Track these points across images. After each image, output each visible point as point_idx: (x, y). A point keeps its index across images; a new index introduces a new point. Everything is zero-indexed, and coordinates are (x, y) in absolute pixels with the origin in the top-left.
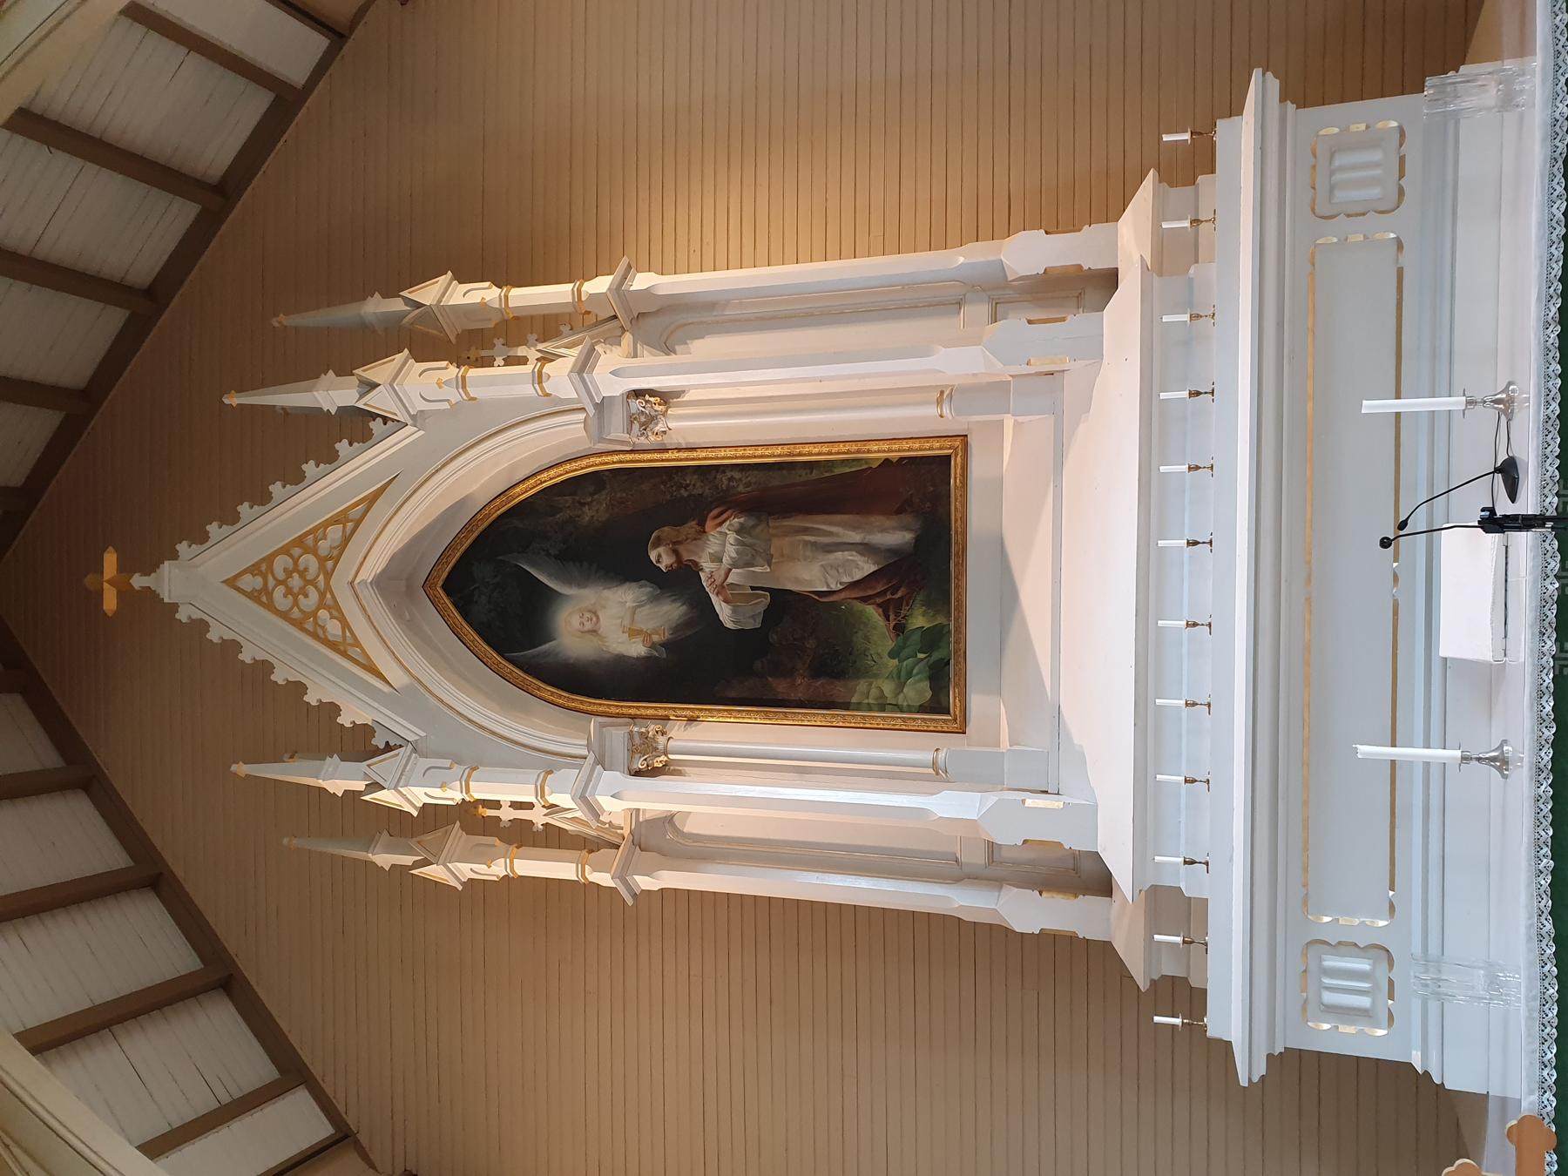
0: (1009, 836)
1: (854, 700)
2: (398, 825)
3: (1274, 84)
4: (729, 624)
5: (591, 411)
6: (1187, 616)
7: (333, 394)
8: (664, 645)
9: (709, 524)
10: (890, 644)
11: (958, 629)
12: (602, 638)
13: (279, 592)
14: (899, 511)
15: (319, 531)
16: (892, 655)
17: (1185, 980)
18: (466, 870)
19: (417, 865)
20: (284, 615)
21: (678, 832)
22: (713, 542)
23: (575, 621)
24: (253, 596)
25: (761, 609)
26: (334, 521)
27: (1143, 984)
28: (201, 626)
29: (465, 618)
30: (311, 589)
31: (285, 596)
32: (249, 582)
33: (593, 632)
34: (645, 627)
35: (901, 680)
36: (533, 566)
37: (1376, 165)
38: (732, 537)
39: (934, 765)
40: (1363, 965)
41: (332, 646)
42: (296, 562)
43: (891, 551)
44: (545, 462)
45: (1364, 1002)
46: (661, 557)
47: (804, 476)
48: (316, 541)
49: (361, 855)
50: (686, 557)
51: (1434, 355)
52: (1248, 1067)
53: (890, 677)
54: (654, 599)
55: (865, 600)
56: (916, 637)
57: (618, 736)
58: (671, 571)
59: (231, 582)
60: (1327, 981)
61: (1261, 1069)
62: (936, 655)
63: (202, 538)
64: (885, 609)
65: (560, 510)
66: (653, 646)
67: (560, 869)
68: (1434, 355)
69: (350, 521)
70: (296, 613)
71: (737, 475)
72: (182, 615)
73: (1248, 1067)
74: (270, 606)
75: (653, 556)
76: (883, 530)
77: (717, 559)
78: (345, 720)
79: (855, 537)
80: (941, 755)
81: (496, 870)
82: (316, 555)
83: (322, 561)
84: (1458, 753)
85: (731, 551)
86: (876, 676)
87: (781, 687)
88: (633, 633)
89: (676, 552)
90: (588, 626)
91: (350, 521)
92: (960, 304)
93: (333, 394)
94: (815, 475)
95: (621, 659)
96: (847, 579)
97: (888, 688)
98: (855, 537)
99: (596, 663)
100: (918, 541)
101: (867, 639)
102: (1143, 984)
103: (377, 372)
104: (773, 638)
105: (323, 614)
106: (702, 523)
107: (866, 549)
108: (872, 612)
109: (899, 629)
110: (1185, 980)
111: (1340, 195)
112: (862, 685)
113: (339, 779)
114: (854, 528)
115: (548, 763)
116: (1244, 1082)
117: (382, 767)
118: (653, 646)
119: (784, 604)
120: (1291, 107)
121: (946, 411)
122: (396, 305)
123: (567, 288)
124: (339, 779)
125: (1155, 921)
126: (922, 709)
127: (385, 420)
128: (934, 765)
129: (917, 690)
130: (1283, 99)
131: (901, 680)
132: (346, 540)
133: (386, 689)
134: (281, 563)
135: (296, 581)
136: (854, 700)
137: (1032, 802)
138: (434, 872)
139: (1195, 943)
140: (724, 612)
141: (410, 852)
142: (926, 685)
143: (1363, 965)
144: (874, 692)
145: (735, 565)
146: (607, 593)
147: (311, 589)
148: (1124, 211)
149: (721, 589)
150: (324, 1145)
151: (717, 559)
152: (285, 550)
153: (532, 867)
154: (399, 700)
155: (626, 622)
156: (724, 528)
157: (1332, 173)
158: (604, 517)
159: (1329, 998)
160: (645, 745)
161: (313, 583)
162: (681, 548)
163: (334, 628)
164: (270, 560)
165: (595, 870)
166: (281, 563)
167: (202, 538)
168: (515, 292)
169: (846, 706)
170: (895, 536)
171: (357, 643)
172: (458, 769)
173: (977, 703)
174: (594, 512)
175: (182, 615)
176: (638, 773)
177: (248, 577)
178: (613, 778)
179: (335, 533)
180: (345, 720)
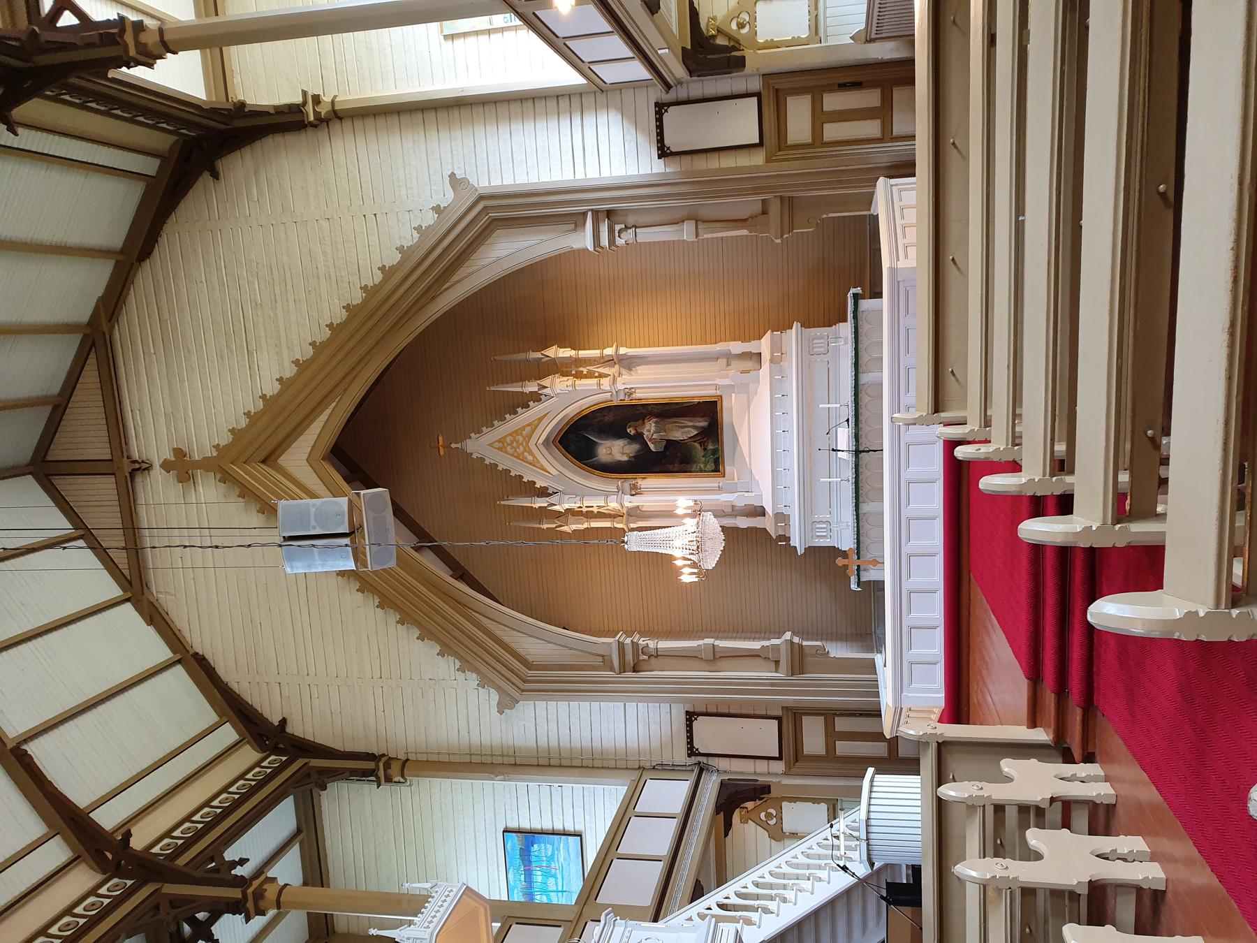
0: (740, 504)
1: (693, 469)
2: (558, 515)
3: (799, 324)
4: (653, 450)
5: (615, 393)
6: (783, 449)
7: (531, 387)
8: (633, 457)
9: (646, 421)
10: (702, 454)
11: (722, 449)
12: (613, 455)
13: (509, 449)
14: (704, 416)
15: (523, 429)
16: (703, 457)
17: (785, 535)
18: (574, 527)
19: (556, 527)
20: (512, 455)
21: (640, 510)
22: (647, 427)
23: (604, 451)
24: (500, 449)
25: (663, 445)
26: (528, 425)
27: (774, 537)
28: (482, 460)
29: (566, 451)
30: (521, 447)
31: (512, 449)
32: (497, 445)
33: (610, 454)
34: (627, 452)
35: (706, 464)
36: (590, 435)
37: (822, 343)
38: (653, 425)
39: (719, 487)
40: (825, 526)
41: (530, 464)
42: (515, 438)
43: (702, 427)
44: (593, 403)
45: (825, 534)
46: (631, 431)
47: (674, 407)
48: (522, 431)
49: (538, 526)
50: (639, 431)
51: (836, 388)
52: (800, 551)
53: (703, 463)
54: (629, 444)
55: (695, 442)
56: (710, 452)
57: (627, 485)
58: (634, 435)
59: (490, 445)
60: (817, 530)
61: (803, 551)
62: (716, 456)
63: (480, 432)
64: (700, 444)
65: (597, 418)
66: (630, 457)
67: (606, 524)
68: (836, 388)
69: (534, 425)
70: (516, 454)
71: (654, 406)
72: (474, 456)
73: (800, 551)
74: (506, 452)
75: (628, 431)
76: (699, 422)
77: (649, 431)
78: (538, 486)
79: (691, 424)
80: (721, 484)
81: (585, 526)
82: (522, 435)
83: (524, 438)
84: (840, 479)
85: (653, 429)
86: (699, 463)
87: (671, 467)
88: (623, 454)
89: (636, 429)
90: (609, 452)
91: (534, 425)
92: (718, 358)
93: (531, 387)
94: (678, 407)
95: (619, 461)
96: (689, 436)
97: (702, 466)
98: (691, 424)
99: (612, 463)
100: (709, 425)
101: (696, 452)
102: (774, 537)
103: (545, 382)
104: (668, 453)
105: (526, 454)
106: (644, 421)
107: (694, 427)
108: (697, 445)
109: (705, 449)
110: (785, 535)
111: (815, 350)
112: (695, 466)
113: (540, 503)
114: (691, 421)
115: (607, 494)
116: (799, 554)
117: (553, 499)
118: (630, 457)
119: (670, 444)
120: (803, 328)
121: (718, 392)
122: (538, 355)
123: (598, 351)
124: (540, 503)
125: (777, 521)
126: (712, 471)
127: (546, 395)
128: (719, 487)
129: (711, 466)
130: (801, 327)
131: (706, 464)
132: (533, 432)
133: (550, 475)
134: (508, 440)
135: (515, 444)
136: (693, 469)
137: (746, 494)
138: (565, 529)
139: (787, 525)
140: (652, 447)
141: (555, 523)
142: (713, 464)
143: (825, 526)
144: (698, 467)
145: (655, 432)
146: (614, 442)
147: (521, 447)
148: (921, 929)
149: (650, 440)
150: (1245, 346)
151: (649, 431)
152: (511, 435)
153: (595, 524)
154: (554, 478)
155: (621, 450)
156: (651, 422)
157: (813, 344)
158: (612, 419)
159: (817, 534)
160: (634, 487)
161: (522, 444)
162: (637, 428)
163: (530, 458)
164: (504, 438)
165: (617, 523)
166: (508, 440)
167: (480, 432)
168: (580, 352)
169: (690, 472)
170: (703, 423)
171: (539, 462)
172: (578, 498)
173: (728, 469)
174: (609, 418)
175: (474, 456)
176: (633, 495)
177: (497, 443)
178: (627, 497)
179: (528, 429)
180: (538, 486)
